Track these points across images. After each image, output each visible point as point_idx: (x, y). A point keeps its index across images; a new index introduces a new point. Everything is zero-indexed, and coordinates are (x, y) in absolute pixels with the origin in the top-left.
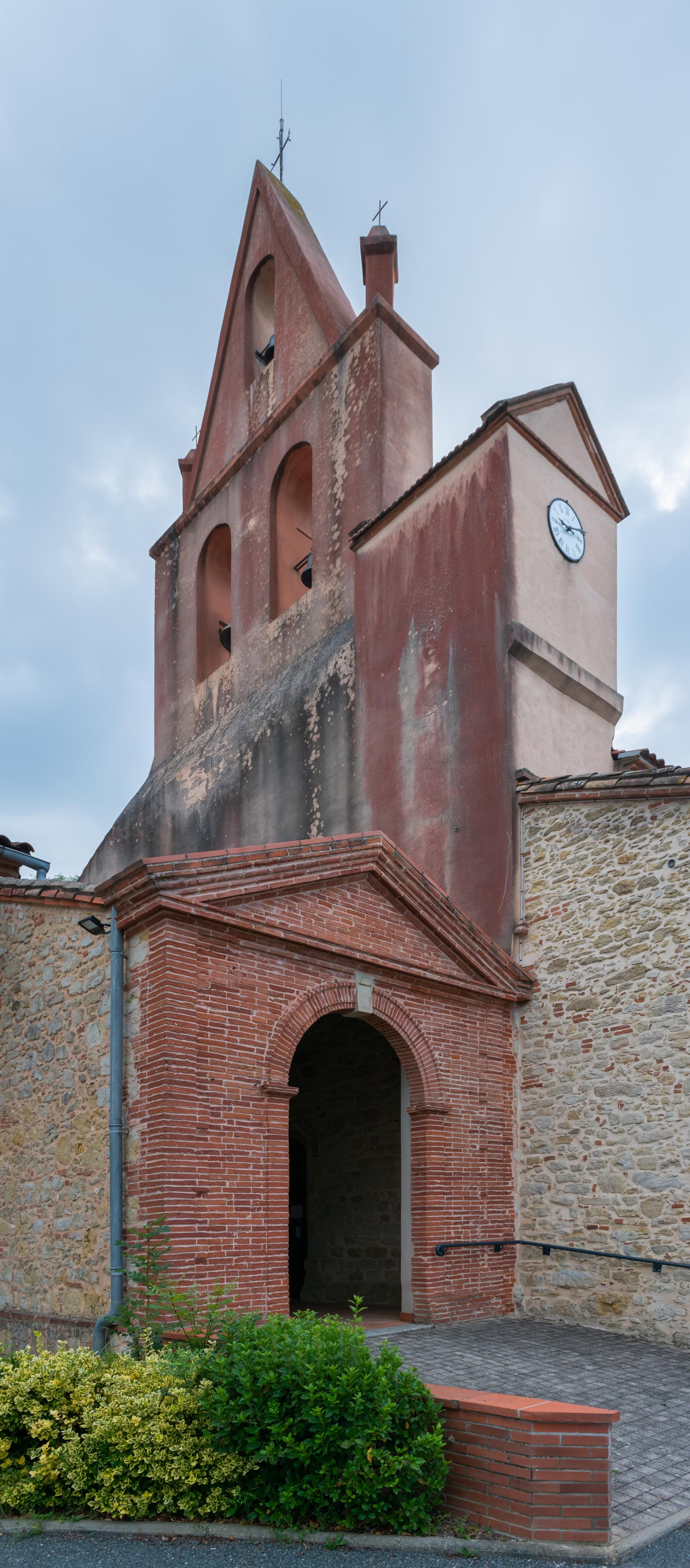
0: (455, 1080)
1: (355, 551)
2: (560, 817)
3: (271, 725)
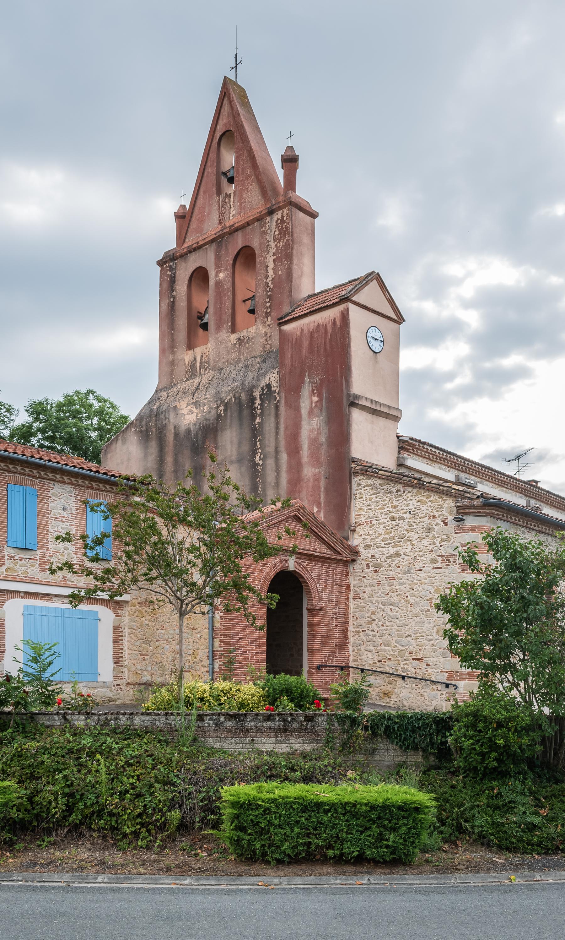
0: (326, 596)
1: (280, 327)
2: (369, 482)
3: (234, 396)
